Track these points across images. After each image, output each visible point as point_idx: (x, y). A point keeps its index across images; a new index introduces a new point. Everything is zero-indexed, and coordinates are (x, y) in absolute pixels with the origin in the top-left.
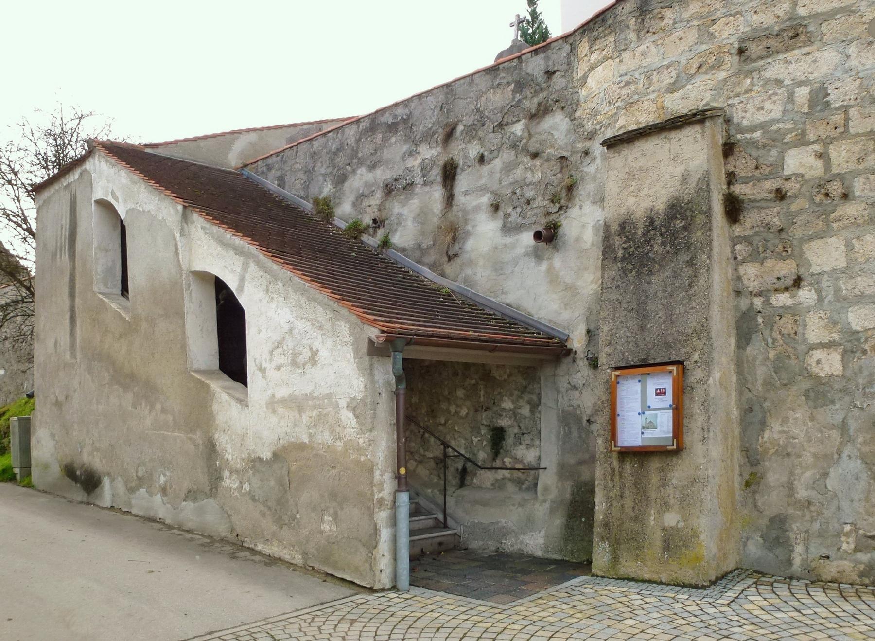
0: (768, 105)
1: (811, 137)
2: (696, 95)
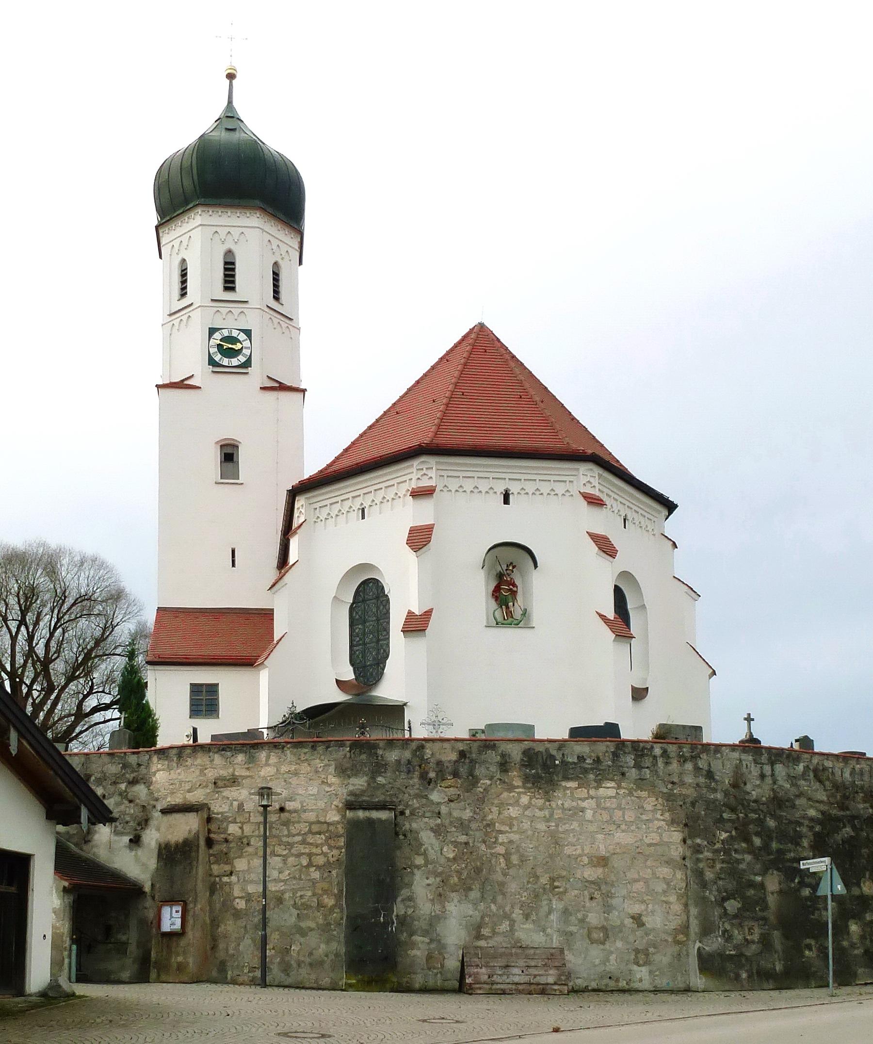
2: (197, 796)
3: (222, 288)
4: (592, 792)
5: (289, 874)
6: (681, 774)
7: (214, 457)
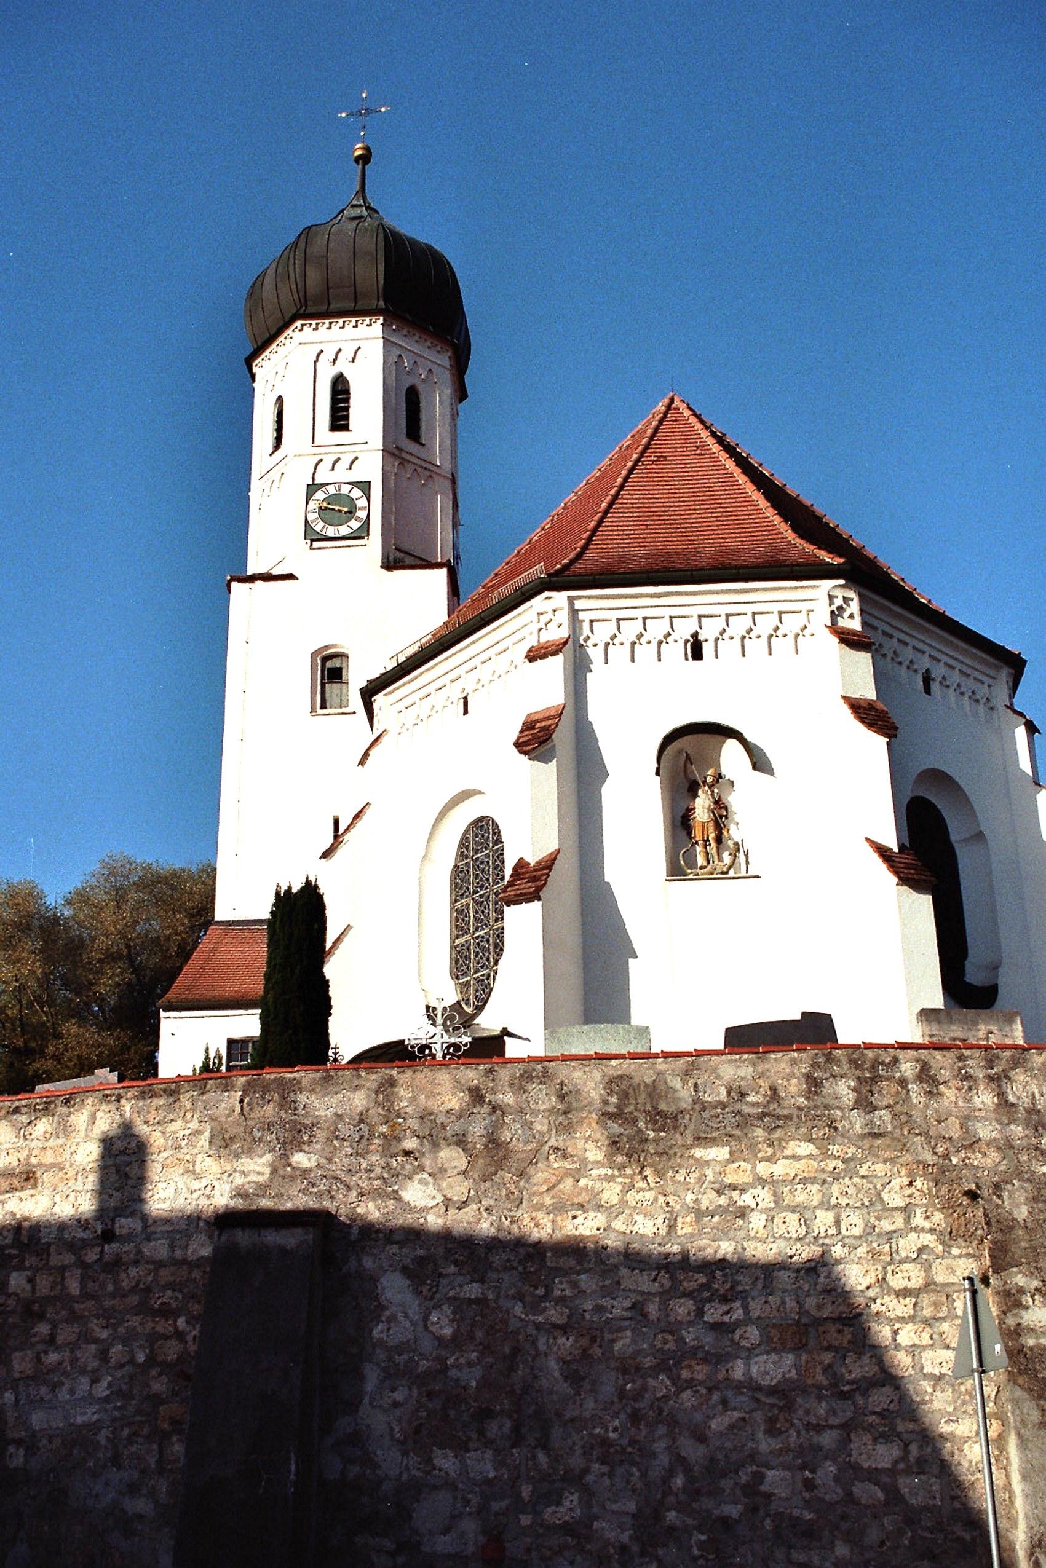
4: (763, 1169)
5: (110, 1385)
6: (968, 1118)
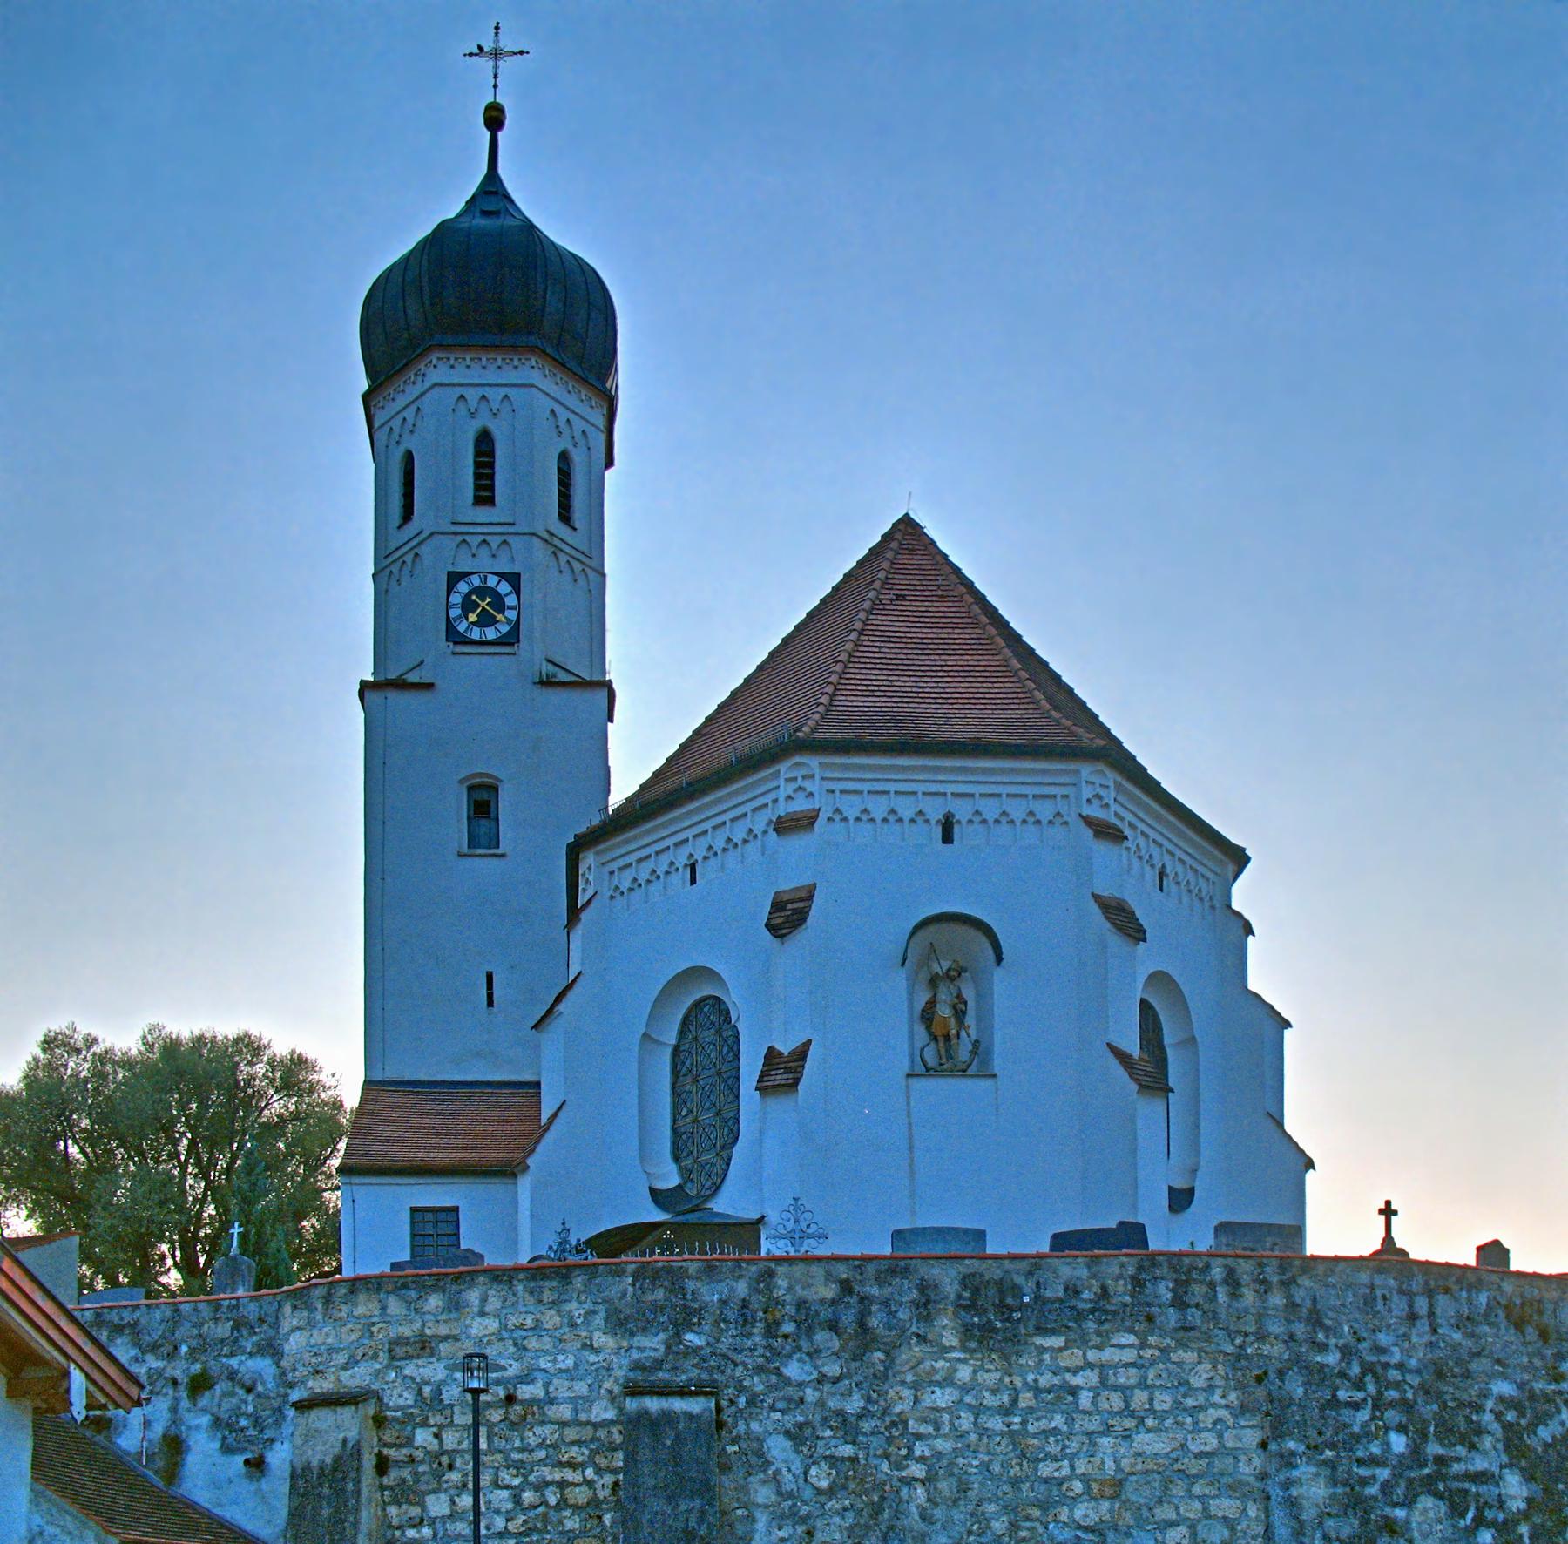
0: (406, 1394)
1: (432, 1422)
2: (358, 1377)
3: (471, 500)
4: (1092, 1355)
7: (459, 804)
